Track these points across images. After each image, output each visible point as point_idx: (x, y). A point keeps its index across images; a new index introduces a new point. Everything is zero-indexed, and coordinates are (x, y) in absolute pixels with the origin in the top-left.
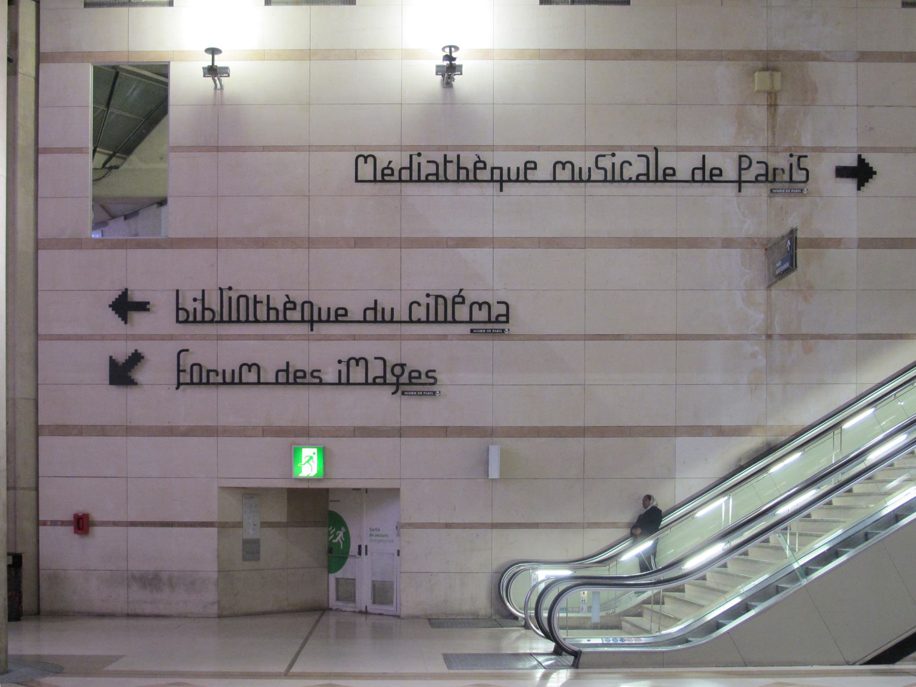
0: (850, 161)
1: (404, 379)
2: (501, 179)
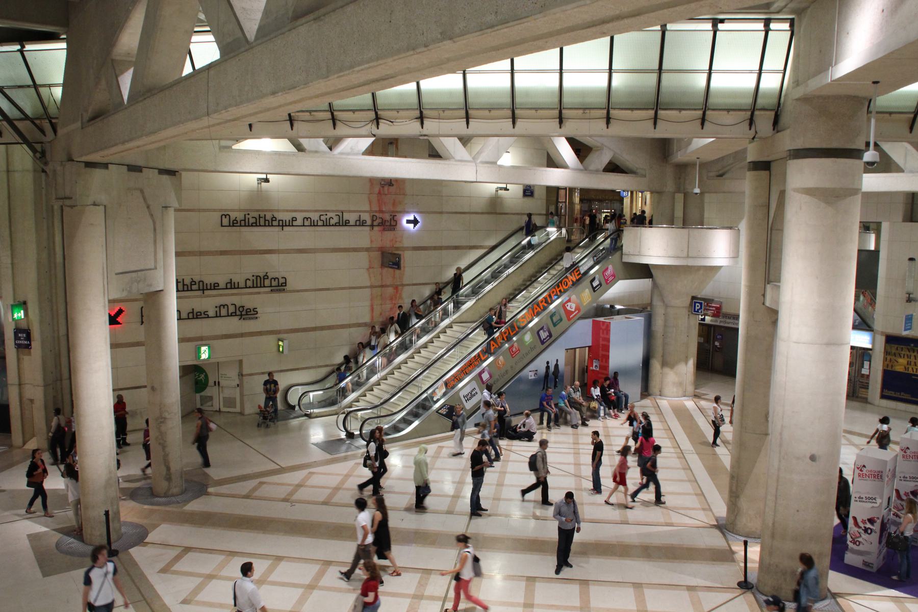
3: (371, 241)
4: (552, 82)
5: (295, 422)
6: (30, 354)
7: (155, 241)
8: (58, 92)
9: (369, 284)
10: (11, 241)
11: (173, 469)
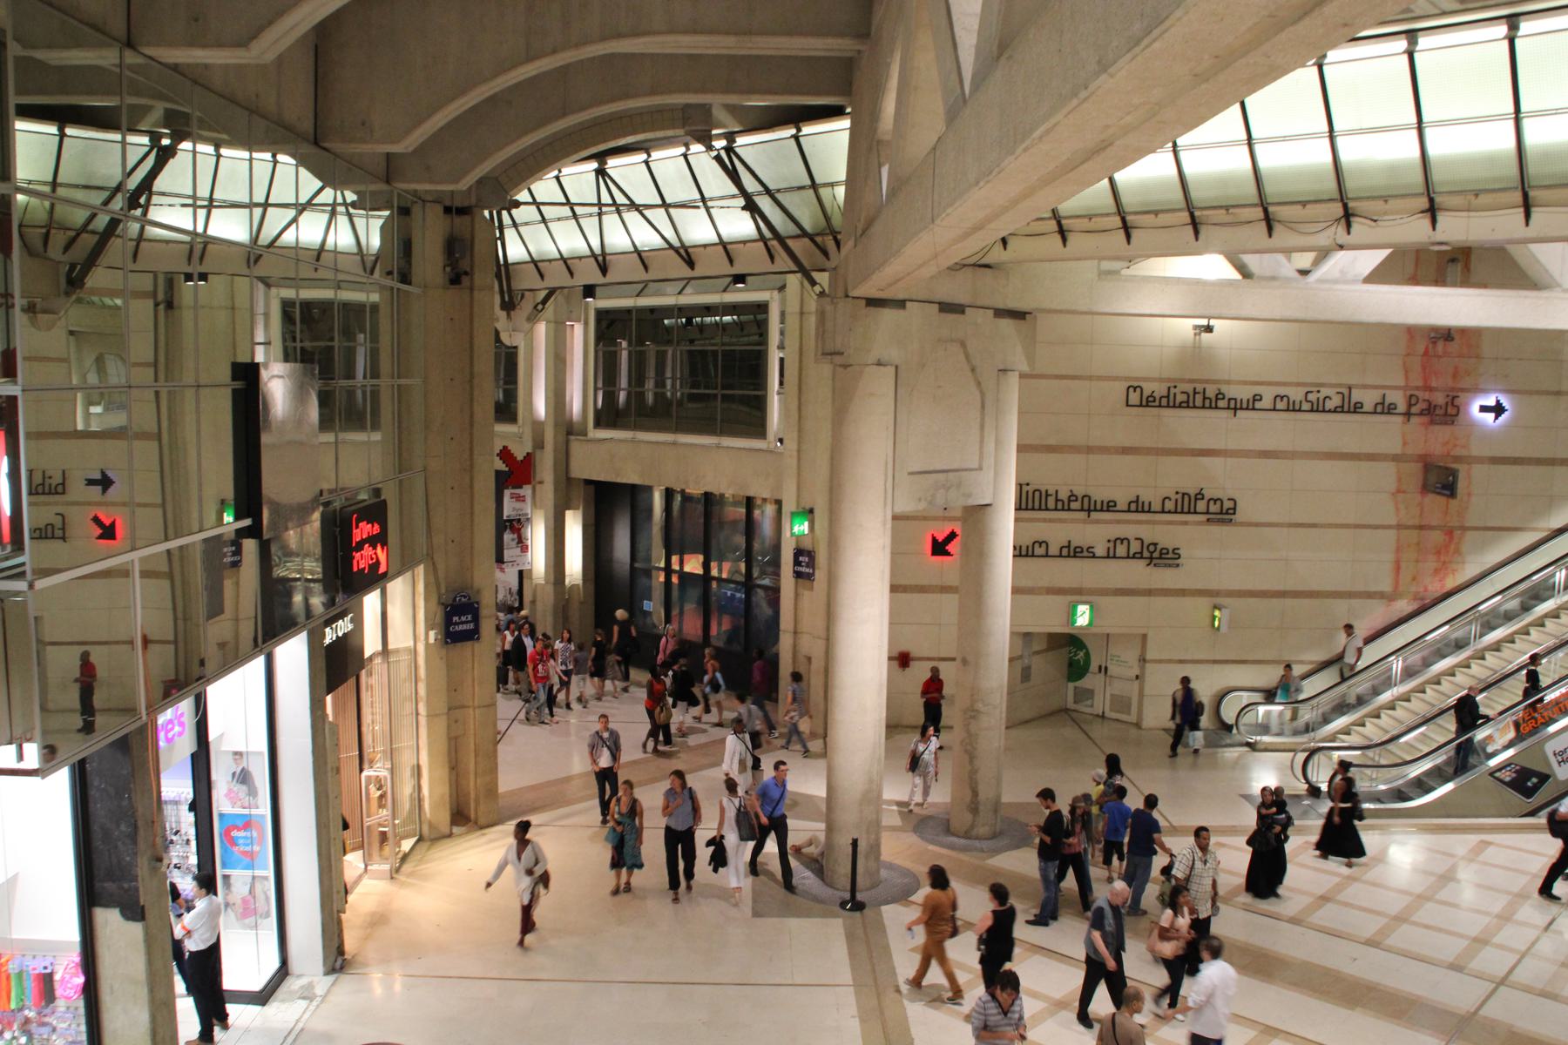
1: (1156, 555)
3: (1405, 444)
4: (1501, 140)
5: (1231, 754)
6: (811, 589)
7: (982, 427)
8: (840, 192)
9: (1393, 522)
10: (800, 417)
11: (982, 797)
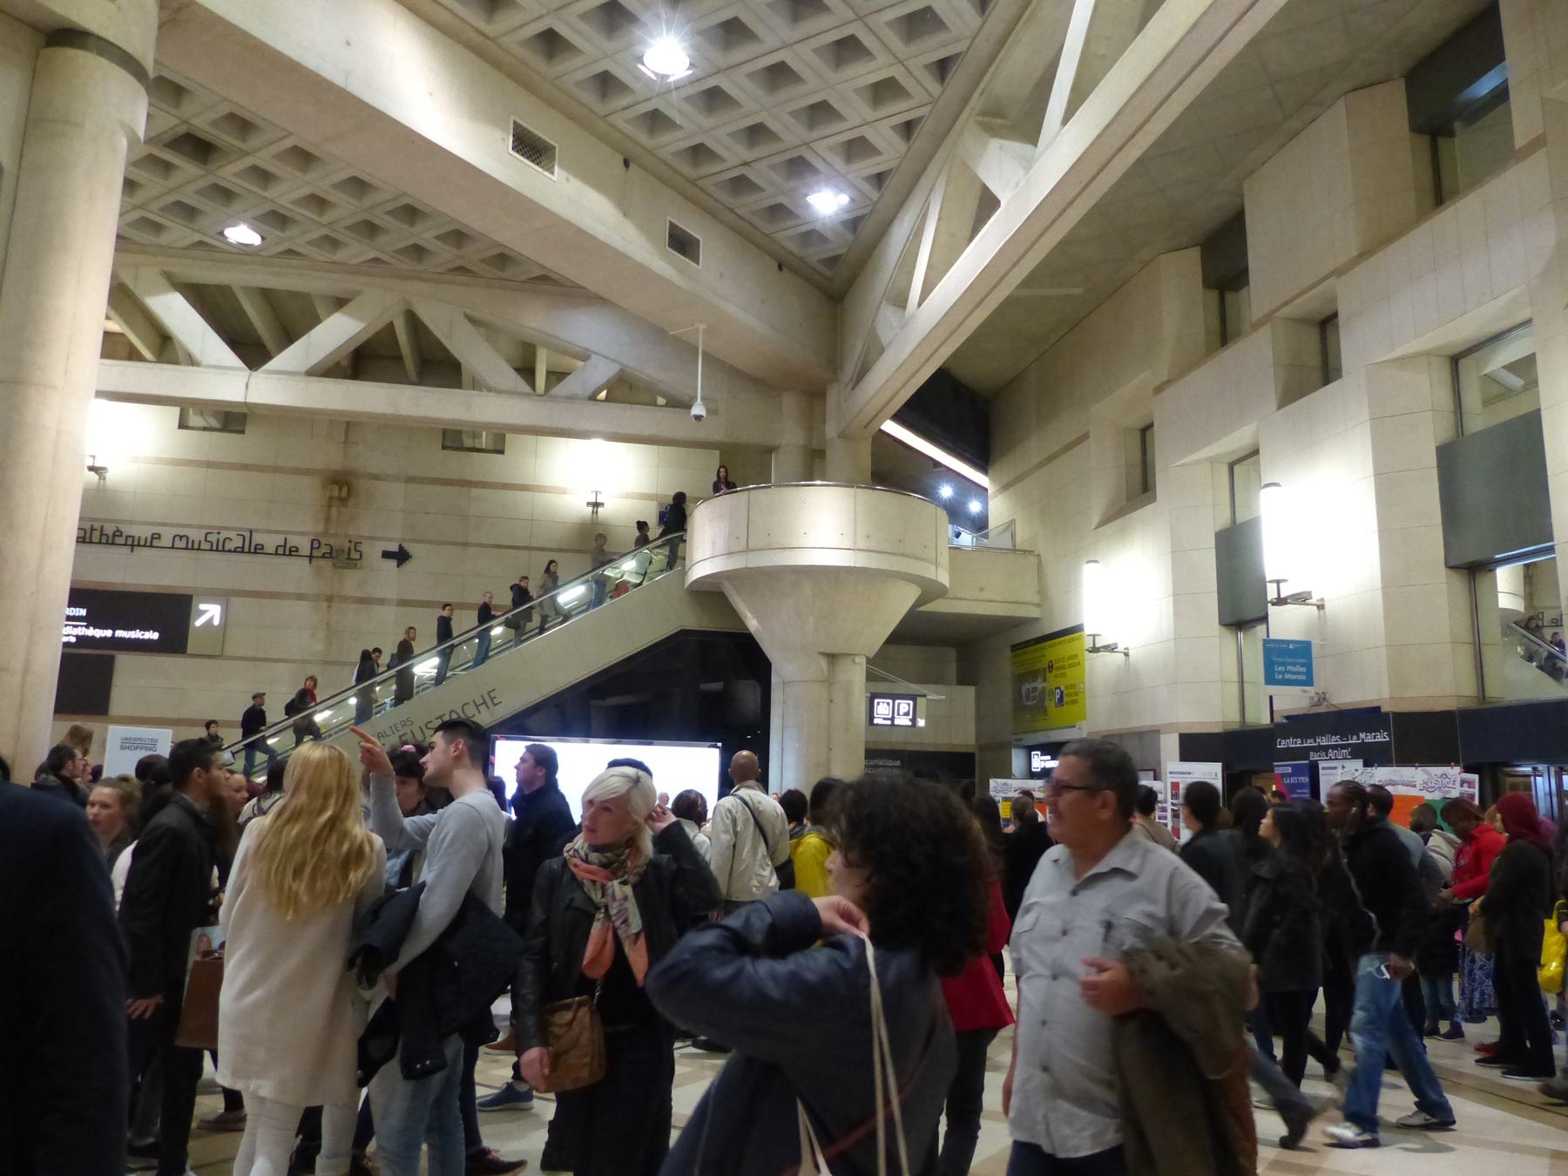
0: (394, 547)
2: (133, 544)
